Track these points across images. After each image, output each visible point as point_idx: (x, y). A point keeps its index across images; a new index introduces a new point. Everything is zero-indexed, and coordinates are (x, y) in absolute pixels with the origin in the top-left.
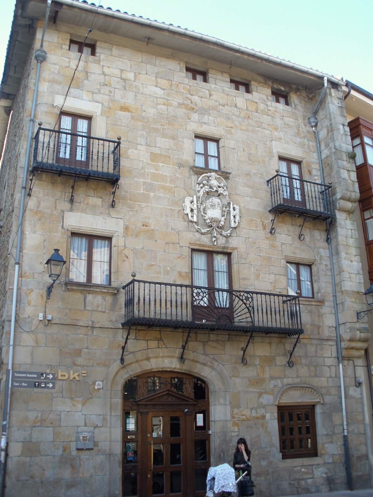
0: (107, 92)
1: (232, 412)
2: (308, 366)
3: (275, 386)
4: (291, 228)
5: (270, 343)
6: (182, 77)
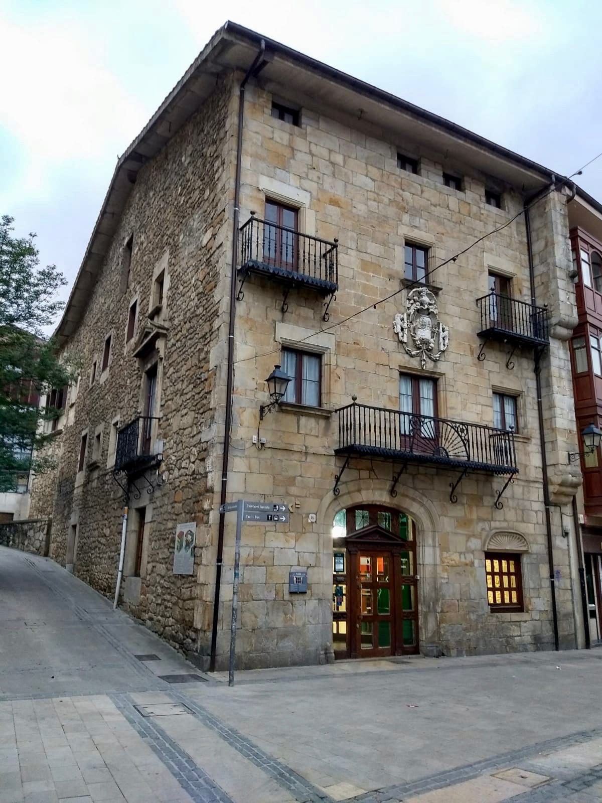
0: (315, 179)
1: (441, 555)
2: (515, 509)
3: (483, 529)
4: (499, 355)
5: (477, 481)
6: (392, 163)
